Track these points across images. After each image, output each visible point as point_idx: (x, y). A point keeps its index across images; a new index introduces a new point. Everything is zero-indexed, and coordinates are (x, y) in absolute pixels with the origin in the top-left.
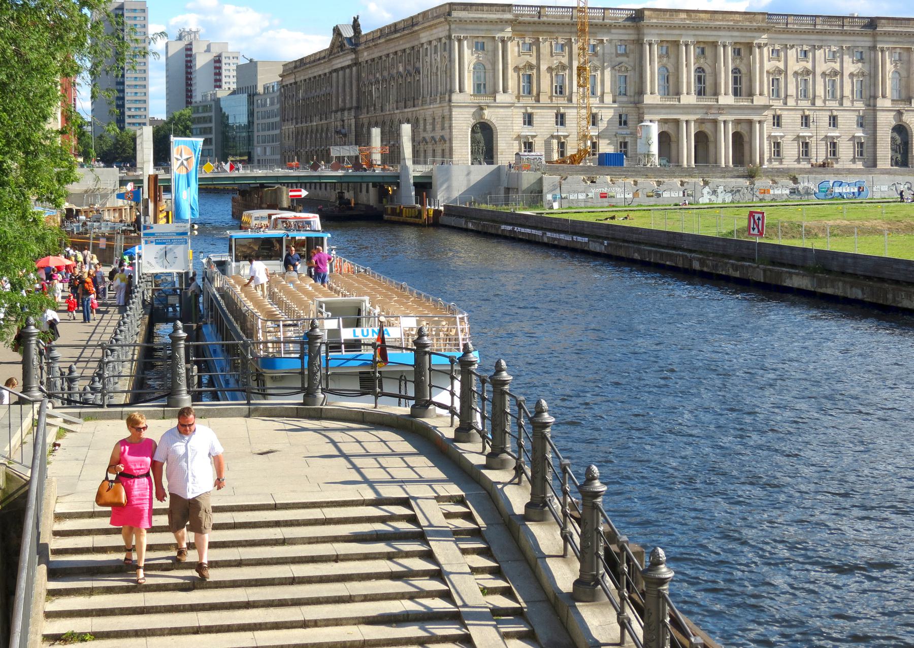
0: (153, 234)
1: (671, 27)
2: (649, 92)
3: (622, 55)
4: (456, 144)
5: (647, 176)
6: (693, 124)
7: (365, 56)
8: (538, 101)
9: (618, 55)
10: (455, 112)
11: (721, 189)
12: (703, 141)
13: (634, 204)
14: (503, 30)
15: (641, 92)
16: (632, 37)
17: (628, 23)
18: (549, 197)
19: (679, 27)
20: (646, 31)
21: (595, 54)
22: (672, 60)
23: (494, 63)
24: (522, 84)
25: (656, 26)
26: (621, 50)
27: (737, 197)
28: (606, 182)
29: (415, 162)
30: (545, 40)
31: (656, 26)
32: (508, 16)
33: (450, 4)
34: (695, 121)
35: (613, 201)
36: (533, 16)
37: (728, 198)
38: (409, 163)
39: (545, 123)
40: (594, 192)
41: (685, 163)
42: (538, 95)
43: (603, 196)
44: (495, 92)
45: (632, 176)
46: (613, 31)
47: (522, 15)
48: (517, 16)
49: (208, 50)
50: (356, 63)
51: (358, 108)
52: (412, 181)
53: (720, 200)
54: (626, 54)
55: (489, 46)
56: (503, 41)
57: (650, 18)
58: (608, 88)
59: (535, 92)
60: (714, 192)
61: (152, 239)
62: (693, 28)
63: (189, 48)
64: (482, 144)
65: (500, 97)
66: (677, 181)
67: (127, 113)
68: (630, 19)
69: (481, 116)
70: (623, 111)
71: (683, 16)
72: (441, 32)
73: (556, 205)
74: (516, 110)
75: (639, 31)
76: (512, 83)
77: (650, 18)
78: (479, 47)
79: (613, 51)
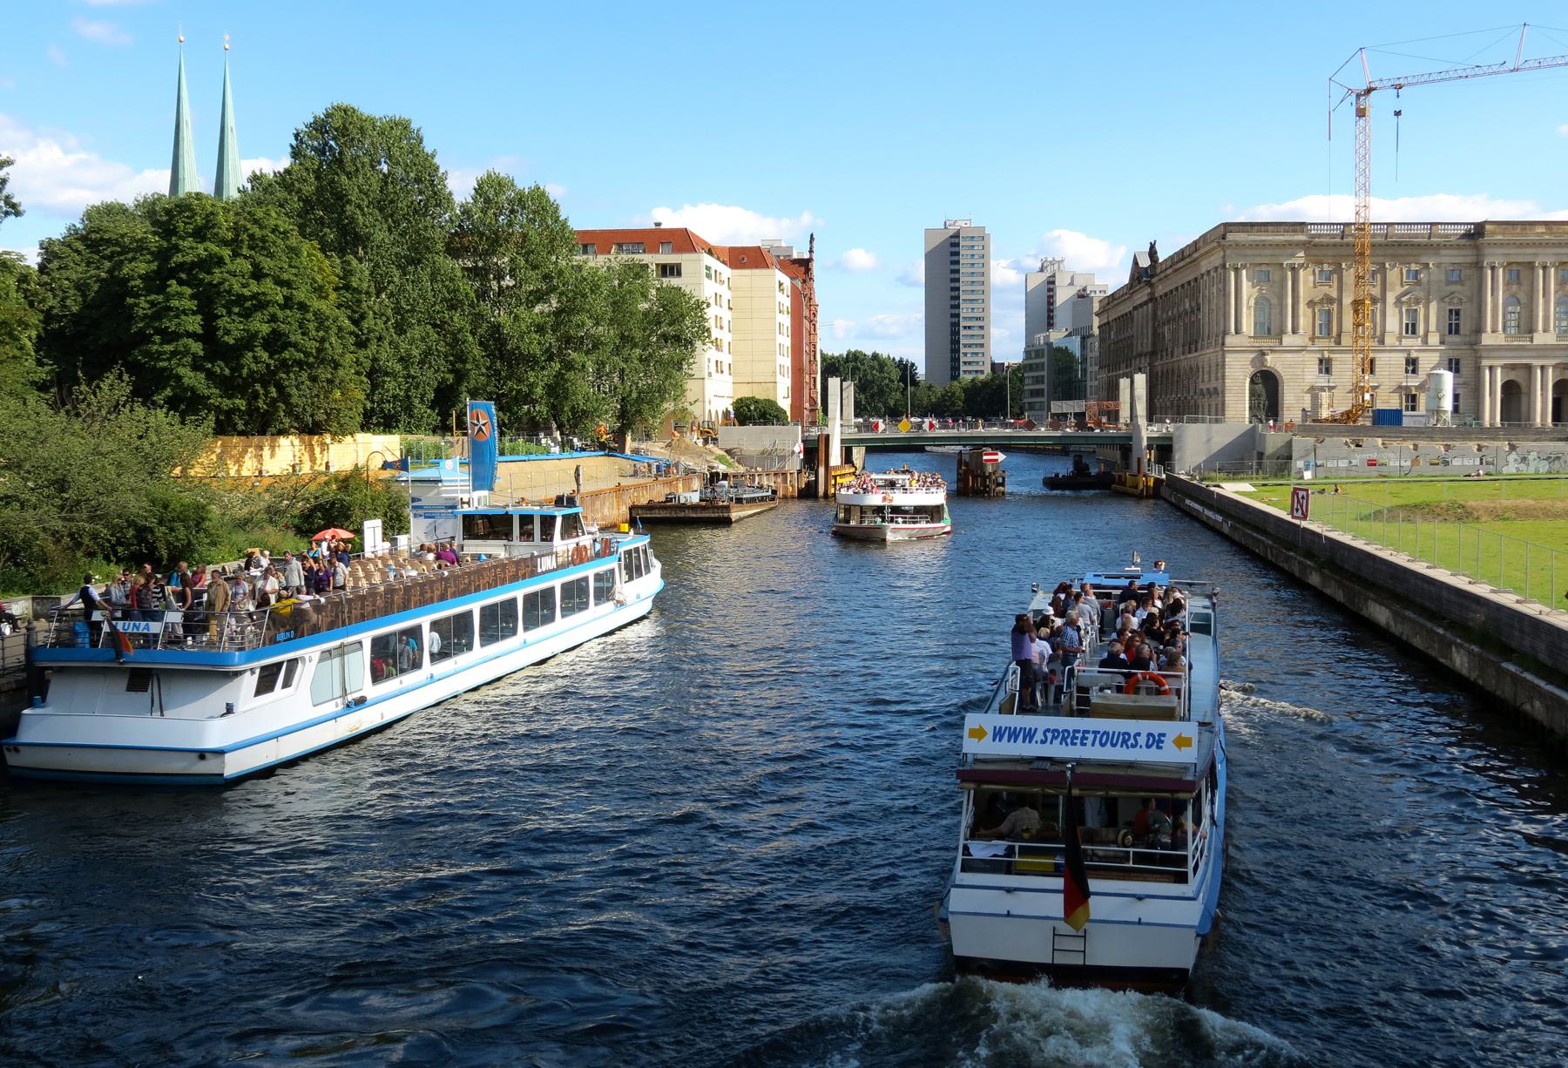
0: (421, 507)
1: (1521, 245)
2: (1489, 329)
3: (1455, 283)
4: (1229, 398)
5: (1432, 439)
6: (1499, 371)
7: (1161, 290)
8: (1338, 343)
9: (1449, 283)
10: (1229, 358)
11: (1533, 455)
12: (1513, 394)
13: (1413, 473)
14: (1293, 255)
15: (1479, 330)
16: (1469, 260)
17: (1463, 242)
18: (1300, 464)
19: (1534, 244)
20: (1487, 251)
21: (1419, 283)
22: (1525, 287)
23: (1281, 297)
24: (1318, 323)
25: (1501, 245)
26: (1455, 277)
27: (1557, 465)
28: (1376, 446)
29: (1150, 420)
30: (1350, 267)
31: (1501, 245)
32: (1302, 238)
33: (1226, 225)
34: (1555, 367)
35: (1384, 470)
36: (1334, 236)
37: (1544, 467)
38: (1142, 421)
39: (1346, 368)
40: (1359, 458)
41: (1538, 420)
42: (1339, 335)
43: (1372, 463)
44: (1282, 332)
45: (1411, 439)
46: (1443, 252)
47: (1320, 236)
48: (1314, 236)
49: (1072, 284)
50: (1152, 299)
51: (1153, 353)
52: (1145, 443)
53: (1531, 470)
54: (1460, 282)
55: (1275, 276)
56: (1293, 269)
57: (1493, 233)
58: (1433, 327)
59: (1335, 333)
60: (1524, 459)
61: (420, 512)
62: (1554, 245)
63: (1051, 281)
64: (1263, 398)
65: (1289, 340)
66: (1473, 446)
67: (962, 359)
68: (1467, 235)
69: (1263, 362)
70: (1454, 355)
71: (1541, 229)
72: (1216, 259)
73: (1308, 475)
74: (1308, 356)
75: (1479, 254)
76: (1304, 322)
77: (1493, 233)
78: (1262, 278)
79: (1443, 277)
